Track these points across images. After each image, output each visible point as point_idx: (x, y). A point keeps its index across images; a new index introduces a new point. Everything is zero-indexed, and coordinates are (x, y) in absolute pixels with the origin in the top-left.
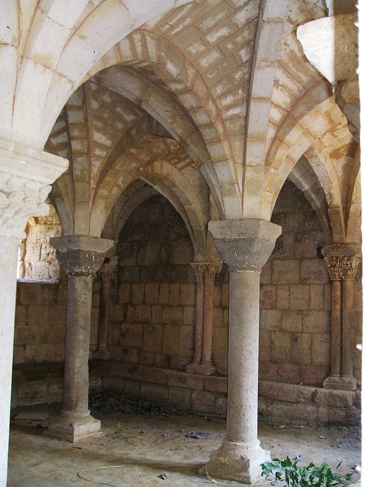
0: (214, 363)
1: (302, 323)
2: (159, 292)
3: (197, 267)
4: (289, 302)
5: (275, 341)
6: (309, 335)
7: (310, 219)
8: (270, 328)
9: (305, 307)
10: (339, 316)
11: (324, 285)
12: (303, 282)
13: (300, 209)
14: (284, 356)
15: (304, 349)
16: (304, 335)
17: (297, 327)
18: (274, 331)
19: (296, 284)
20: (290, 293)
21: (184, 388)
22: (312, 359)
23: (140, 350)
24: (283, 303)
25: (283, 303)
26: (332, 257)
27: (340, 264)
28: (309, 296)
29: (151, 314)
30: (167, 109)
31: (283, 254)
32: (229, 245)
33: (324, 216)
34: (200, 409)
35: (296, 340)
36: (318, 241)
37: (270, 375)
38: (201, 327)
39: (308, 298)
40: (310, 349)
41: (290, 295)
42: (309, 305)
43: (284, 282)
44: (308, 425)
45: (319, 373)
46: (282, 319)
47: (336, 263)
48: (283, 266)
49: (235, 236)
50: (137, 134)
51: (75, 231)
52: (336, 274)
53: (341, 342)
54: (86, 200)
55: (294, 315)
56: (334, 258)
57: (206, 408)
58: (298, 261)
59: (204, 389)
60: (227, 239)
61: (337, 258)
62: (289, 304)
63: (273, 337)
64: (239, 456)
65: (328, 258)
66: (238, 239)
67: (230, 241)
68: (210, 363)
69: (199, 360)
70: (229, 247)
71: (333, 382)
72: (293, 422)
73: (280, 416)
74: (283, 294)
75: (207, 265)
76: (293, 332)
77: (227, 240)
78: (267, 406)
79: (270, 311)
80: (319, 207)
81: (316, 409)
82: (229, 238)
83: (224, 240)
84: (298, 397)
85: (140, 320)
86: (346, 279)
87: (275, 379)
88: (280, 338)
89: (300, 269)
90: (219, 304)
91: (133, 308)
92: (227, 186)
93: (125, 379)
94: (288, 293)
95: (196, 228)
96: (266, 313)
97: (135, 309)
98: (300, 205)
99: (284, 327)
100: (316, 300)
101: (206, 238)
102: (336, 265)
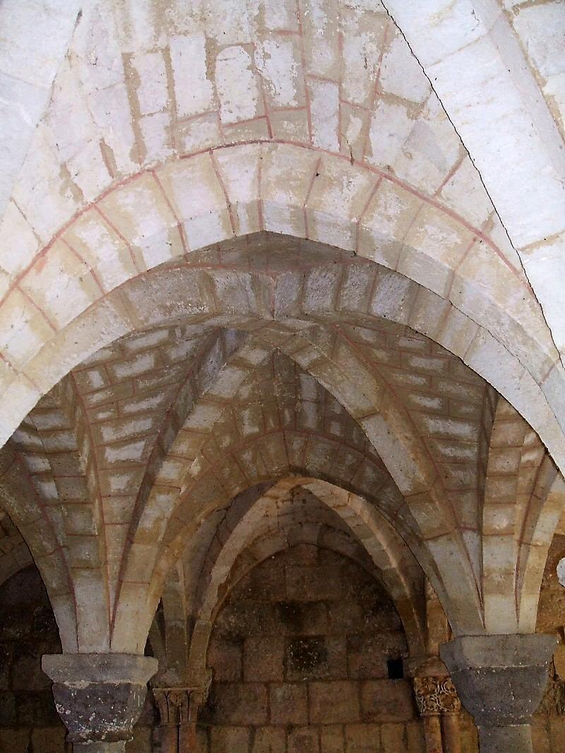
3: (166, 697)
7: (373, 614)
12: (367, 718)
20: (345, 738)
26: (427, 678)
27: (441, 689)
30: (407, 435)
31: (328, 670)
41: (345, 744)
43: (332, 721)
48: (329, 692)
49: (509, 664)
50: (254, 461)
52: (435, 705)
54: (145, 580)
56: (431, 679)
60: (495, 669)
61: (435, 678)
65: (420, 680)
67: (501, 672)
77: (494, 671)
80: (409, 597)
82: (499, 668)
83: (489, 670)
86: (449, 714)
89: (360, 697)
92: (497, 578)
94: (341, 739)
101: (190, 643)
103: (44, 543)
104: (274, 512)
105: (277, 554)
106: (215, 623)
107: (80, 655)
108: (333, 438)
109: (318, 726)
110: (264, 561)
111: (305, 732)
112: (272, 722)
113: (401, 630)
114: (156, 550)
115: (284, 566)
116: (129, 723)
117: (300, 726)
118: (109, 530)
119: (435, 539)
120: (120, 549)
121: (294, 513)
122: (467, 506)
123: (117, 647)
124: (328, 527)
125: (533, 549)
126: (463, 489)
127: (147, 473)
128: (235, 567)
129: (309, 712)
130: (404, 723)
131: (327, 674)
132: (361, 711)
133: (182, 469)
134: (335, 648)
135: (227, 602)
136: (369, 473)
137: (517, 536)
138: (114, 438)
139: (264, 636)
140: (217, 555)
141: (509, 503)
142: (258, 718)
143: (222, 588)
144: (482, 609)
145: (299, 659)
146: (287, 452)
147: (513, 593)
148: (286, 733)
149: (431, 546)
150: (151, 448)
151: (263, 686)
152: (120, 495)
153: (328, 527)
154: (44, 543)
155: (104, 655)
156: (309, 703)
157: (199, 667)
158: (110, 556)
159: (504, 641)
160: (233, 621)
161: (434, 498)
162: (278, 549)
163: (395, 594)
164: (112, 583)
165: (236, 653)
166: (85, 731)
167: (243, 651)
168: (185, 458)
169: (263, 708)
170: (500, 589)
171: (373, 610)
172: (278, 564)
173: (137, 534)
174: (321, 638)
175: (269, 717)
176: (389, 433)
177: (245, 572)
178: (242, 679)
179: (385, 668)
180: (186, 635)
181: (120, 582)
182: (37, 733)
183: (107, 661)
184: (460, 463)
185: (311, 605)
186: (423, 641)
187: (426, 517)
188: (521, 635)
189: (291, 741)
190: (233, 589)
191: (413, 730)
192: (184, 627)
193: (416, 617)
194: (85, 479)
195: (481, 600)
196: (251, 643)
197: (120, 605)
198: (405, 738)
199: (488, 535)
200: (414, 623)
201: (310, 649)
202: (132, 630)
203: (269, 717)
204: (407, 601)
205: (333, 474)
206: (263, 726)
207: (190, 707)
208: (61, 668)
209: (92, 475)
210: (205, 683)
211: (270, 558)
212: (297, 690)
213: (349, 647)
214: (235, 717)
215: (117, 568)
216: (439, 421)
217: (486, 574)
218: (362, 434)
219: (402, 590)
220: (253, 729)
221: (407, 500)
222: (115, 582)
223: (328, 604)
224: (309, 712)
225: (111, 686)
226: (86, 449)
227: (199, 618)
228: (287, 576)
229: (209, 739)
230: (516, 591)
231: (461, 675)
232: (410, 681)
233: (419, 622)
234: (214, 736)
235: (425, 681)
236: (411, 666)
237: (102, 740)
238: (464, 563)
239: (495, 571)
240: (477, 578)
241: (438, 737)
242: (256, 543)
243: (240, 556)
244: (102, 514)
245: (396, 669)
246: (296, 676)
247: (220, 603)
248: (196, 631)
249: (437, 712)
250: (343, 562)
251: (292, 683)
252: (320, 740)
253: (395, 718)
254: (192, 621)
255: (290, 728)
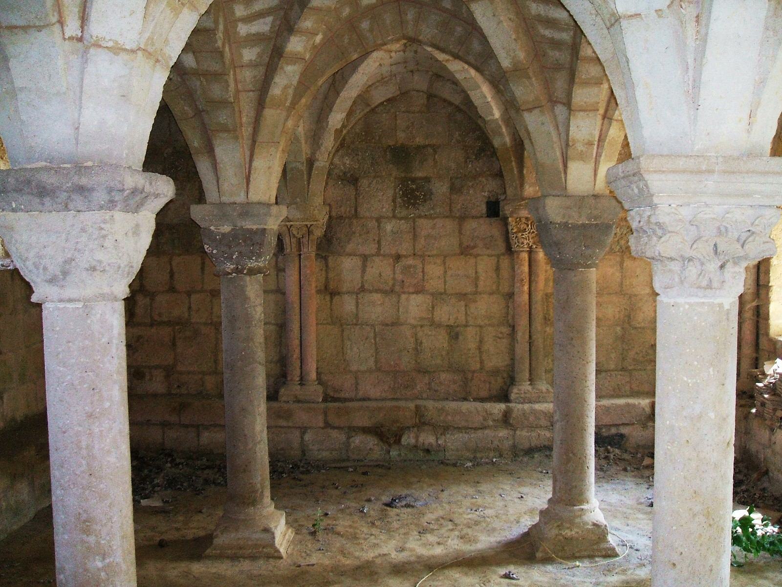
0: (320, 381)
1: (466, 313)
2: (203, 269)
3: (289, 230)
4: (445, 282)
5: (424, 341)
6: (478, 329)
8: (413, 322)
9: (470, 289)
10: (527, 301)
11: (498, 256)
12: (465, 251)
13: (459, 142)
14: (439, 361)
15: (470, 350)
16: (469, 329)
17: (457, 318)
18: (422, 326)
19: (455, 255)
21: (289, 427)
22: (482, 362)
23: (169, 371)
24: (434, 284)
25: (434, 284)
27: (531, 229)
28: (476, 272)
29: (190, 308)
31: (433, 209)
32: (574, 233)
33: (513, 159)
34: (320, 457)
35: (457, 338)
36: (488, 191)
37: (416, 391)
38: (298, 325)
39: (474, 275)
40: (479, 348)
41: (445, 272)
42: (477, 286)
43: (435, 252)
44: (501, 456)
45: (493, 382)
46: (433, 308)
47: (525, 226)
49: (583, 220)
50: (371, 30)
51: (250, 195)
52: (525, 242)
53: (530, 337)
54: (275, 140)
55: (453, 300)
56: (524, 220)
57: (331, 453)
58: (457, 220)
59: (327, 425)
60: (571, 224)
62: (445, 285)
63: (420, 334)
64: (591, 523)
66: (587, 224)
67: (575, 227)
68: (316, 383)
69: (298, 379)
70: (574, 235)
71: (525, 393)
72: (478, 455)
73: (457, 450)
74: (434, 270)
75: (309, 226)
76: (451, 326)
78: (437, 439)
79: (414, 296)
81: (511, 433)
83: (566, 225)
84: (485, 419)
85: (165, 319)
87: (425, 396)
88: (431, 335)
89: (460, 232)
90: (323, 288)
91: (148, 299)
92: (580, 147)
93: (165, 425)
94: (442, 268)
95: (294, 165)
96: (408, 300)
97: (152, 300)
98: (460, 135)
99: (437, 319)
100: (486, 280)
101: (309, 183)
102: (525, 229)
103: (186, 108)
104: (387, 61)
105: (389, 100)
106: (331, 163)
107: (222, 205)
108: (445, 10)
109: (423, 257)
110: (376, 107)
111: (410, 262)
112: (382, 252)
113: (500, 175)
114: (284, 114)
115: (396, 112)
116: (265, 260)
117: (406, 257)
118: (243, 96)
119: (530, 110)
120: (252, 114)
121: (405, 62)
122: (560, 83)
123: (254, 197)
124: (438, 76)
125: (614, 123)
126: (557, 67)
127: (275, 45)
128: (350, 113)
129: (414, 246)
130: (498, 256)
131: (432, 212)
132: (461, 245)
133: (307, 43)
134: (440, 188)
135: (342, 145)
136: (476, 46)
137: (602, 111)
138: (245, 14)
139: (375, 177)
140: (333, 103)
141: (596, 84)
142: (370, 248)
143: (338, 132)
144: (566, 173)
145: (407, 197)
146: (402, 22)
147: (594, 160)
148: (394, 262)
149: (526, 115)
150: (278, 22)
151: (374, 221)
152: (252, 65)
153: (438, 76)
154: (186, 108)
155: (242, 205)
156: (415, 237)
157: (318, 204)
158: (244, 119)
159: (581, 200)
160: (348, 162)
161: (531, 74)
162: (390, 96)
163: (496, 142)
164: (247, 143)
165: (350, 191)
166: (230, 267)
167: (357, 190)
168: (310, 33)
169: (374, 240)
170: (582, 157)
171: (476, 155)
172: (389, 110)
173: (268, 100)
174: (427, 180)
175: (379, 249)
176: (494, 15)
177: (359, 117)
178: (356, 215)
179: (483, 208)
180: (305, 177)
181: (254, 142)
182: (176, 260)
183: (247, 209)
184: (556, 44)
185: (419, 148)
186: (519, 186)
187: (525, 91)
188: (596, 196)
189: (398, 270)
190: (348, 132)
191: (505, 262)
192: (304, 168)
193: (513, 163)
194: (221, 54)
195: (565, 166)
196: (364, 183)
197: (255, 162)
198: (497, 269)
199: (576, 110)
200: (512, 170)
201: (417, 189)
202: (265, 183)
203: (379, 249)
204: (507, 149)
205: (442, 45)
206: (373, 255)
207: (310, 239)
208: (208, 216)
209: (227, 49)
210: (322, 218)
211: (382, 103)
212: (404, 225)
213: (453, 189)
214: (350, 247)
215: (250, 130)
216: (541, 5)
217: (571, 144)
218: (471, 13)
219: (503, 139)
220: (365, 258)
221: (507, 75)
222: (250, 142)
223: (435, 148)
224: (414, 246)
225: (250, 231)
226: (221, 27)
227: (318, 160)
228: (398, 122)
229: (327, 266)
230: (596, 158)
231: (543, 228)
232: (505, 220)
233: (517, 168)
234: (331, 264)
235: (519, 220)
236: (506, 208)
237: (244, 274)
238: (554, 134)
239: (578, 141)
240: (564, 146)
241: (526, 269)
242: (370, 90)
243: (354, 102)
244: (236, 80)
245: (494, 209)
246: (404, 213)
247: (337, 145)
248: (314, 172)
249: (527, 248)
250: (450, 109)
251: (401, 219)
252: (423, 268)
253: (489, 252)
254: (311, 163)
255: (398, 257)
